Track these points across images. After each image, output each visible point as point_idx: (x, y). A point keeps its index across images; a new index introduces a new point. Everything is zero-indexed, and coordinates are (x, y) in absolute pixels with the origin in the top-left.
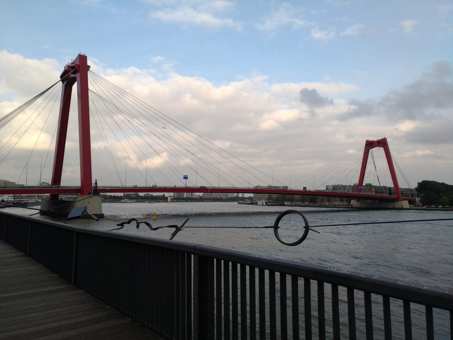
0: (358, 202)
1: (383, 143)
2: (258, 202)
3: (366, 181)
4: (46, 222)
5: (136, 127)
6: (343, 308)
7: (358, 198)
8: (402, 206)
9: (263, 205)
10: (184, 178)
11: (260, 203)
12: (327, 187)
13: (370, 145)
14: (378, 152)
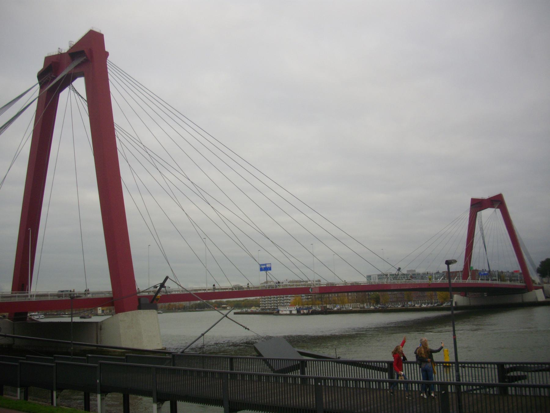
0: (465, 298)
1: (497, 202)
2: (281, 309)
3: (42, 284)
4: (484, 284)
5: (200, 195)
6: (534, 378)
7: (464, 290)
8: (537, 298)
9: (291, 314)
10: (261, 270)
11: (284, 310)
12: (369, 277)
13: (478, 205)
14: (489, 217)
